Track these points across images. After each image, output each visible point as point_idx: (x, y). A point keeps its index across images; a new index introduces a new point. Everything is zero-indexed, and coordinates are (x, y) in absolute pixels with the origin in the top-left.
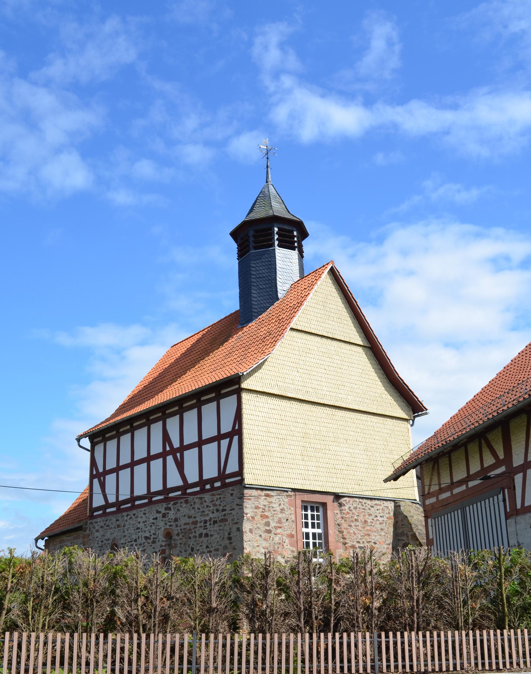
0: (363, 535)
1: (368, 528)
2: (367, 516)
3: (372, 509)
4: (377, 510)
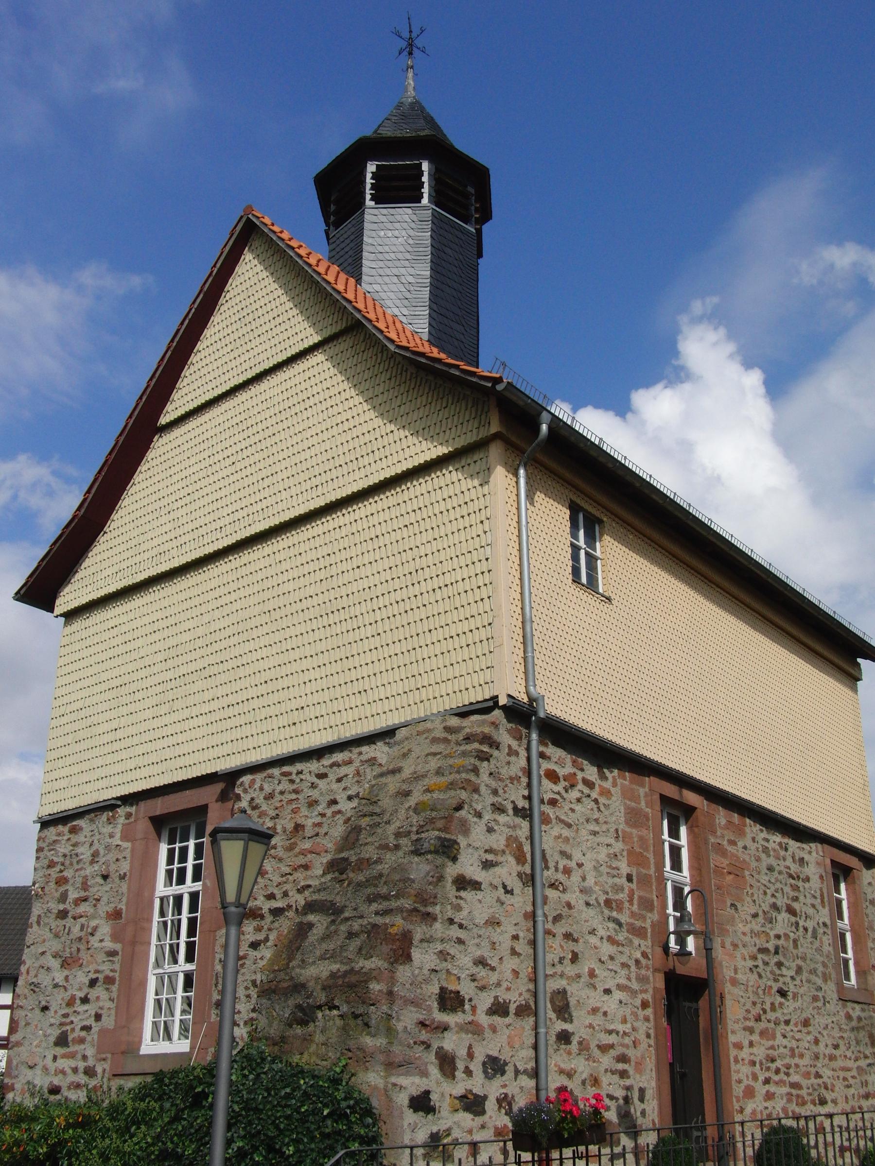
0: (288, 870)
1: (307, 845)
2: (304, 811)
3: (322, 784)
4: (339, 780)
